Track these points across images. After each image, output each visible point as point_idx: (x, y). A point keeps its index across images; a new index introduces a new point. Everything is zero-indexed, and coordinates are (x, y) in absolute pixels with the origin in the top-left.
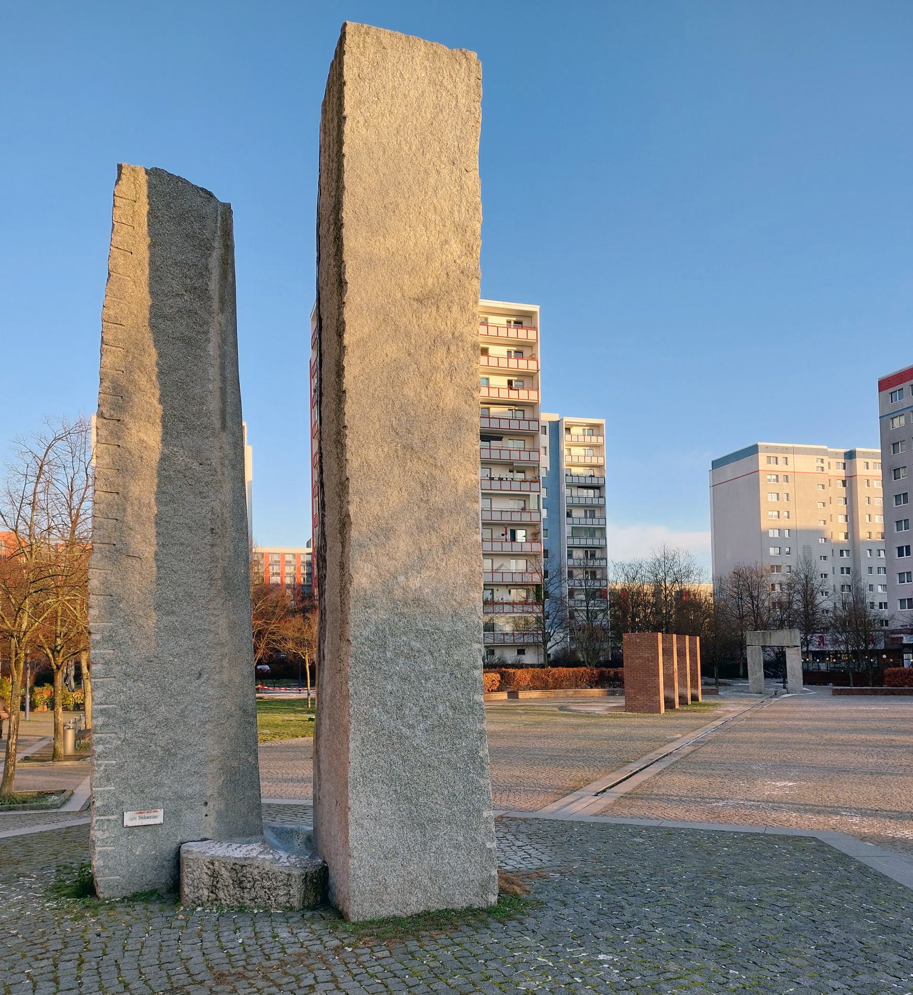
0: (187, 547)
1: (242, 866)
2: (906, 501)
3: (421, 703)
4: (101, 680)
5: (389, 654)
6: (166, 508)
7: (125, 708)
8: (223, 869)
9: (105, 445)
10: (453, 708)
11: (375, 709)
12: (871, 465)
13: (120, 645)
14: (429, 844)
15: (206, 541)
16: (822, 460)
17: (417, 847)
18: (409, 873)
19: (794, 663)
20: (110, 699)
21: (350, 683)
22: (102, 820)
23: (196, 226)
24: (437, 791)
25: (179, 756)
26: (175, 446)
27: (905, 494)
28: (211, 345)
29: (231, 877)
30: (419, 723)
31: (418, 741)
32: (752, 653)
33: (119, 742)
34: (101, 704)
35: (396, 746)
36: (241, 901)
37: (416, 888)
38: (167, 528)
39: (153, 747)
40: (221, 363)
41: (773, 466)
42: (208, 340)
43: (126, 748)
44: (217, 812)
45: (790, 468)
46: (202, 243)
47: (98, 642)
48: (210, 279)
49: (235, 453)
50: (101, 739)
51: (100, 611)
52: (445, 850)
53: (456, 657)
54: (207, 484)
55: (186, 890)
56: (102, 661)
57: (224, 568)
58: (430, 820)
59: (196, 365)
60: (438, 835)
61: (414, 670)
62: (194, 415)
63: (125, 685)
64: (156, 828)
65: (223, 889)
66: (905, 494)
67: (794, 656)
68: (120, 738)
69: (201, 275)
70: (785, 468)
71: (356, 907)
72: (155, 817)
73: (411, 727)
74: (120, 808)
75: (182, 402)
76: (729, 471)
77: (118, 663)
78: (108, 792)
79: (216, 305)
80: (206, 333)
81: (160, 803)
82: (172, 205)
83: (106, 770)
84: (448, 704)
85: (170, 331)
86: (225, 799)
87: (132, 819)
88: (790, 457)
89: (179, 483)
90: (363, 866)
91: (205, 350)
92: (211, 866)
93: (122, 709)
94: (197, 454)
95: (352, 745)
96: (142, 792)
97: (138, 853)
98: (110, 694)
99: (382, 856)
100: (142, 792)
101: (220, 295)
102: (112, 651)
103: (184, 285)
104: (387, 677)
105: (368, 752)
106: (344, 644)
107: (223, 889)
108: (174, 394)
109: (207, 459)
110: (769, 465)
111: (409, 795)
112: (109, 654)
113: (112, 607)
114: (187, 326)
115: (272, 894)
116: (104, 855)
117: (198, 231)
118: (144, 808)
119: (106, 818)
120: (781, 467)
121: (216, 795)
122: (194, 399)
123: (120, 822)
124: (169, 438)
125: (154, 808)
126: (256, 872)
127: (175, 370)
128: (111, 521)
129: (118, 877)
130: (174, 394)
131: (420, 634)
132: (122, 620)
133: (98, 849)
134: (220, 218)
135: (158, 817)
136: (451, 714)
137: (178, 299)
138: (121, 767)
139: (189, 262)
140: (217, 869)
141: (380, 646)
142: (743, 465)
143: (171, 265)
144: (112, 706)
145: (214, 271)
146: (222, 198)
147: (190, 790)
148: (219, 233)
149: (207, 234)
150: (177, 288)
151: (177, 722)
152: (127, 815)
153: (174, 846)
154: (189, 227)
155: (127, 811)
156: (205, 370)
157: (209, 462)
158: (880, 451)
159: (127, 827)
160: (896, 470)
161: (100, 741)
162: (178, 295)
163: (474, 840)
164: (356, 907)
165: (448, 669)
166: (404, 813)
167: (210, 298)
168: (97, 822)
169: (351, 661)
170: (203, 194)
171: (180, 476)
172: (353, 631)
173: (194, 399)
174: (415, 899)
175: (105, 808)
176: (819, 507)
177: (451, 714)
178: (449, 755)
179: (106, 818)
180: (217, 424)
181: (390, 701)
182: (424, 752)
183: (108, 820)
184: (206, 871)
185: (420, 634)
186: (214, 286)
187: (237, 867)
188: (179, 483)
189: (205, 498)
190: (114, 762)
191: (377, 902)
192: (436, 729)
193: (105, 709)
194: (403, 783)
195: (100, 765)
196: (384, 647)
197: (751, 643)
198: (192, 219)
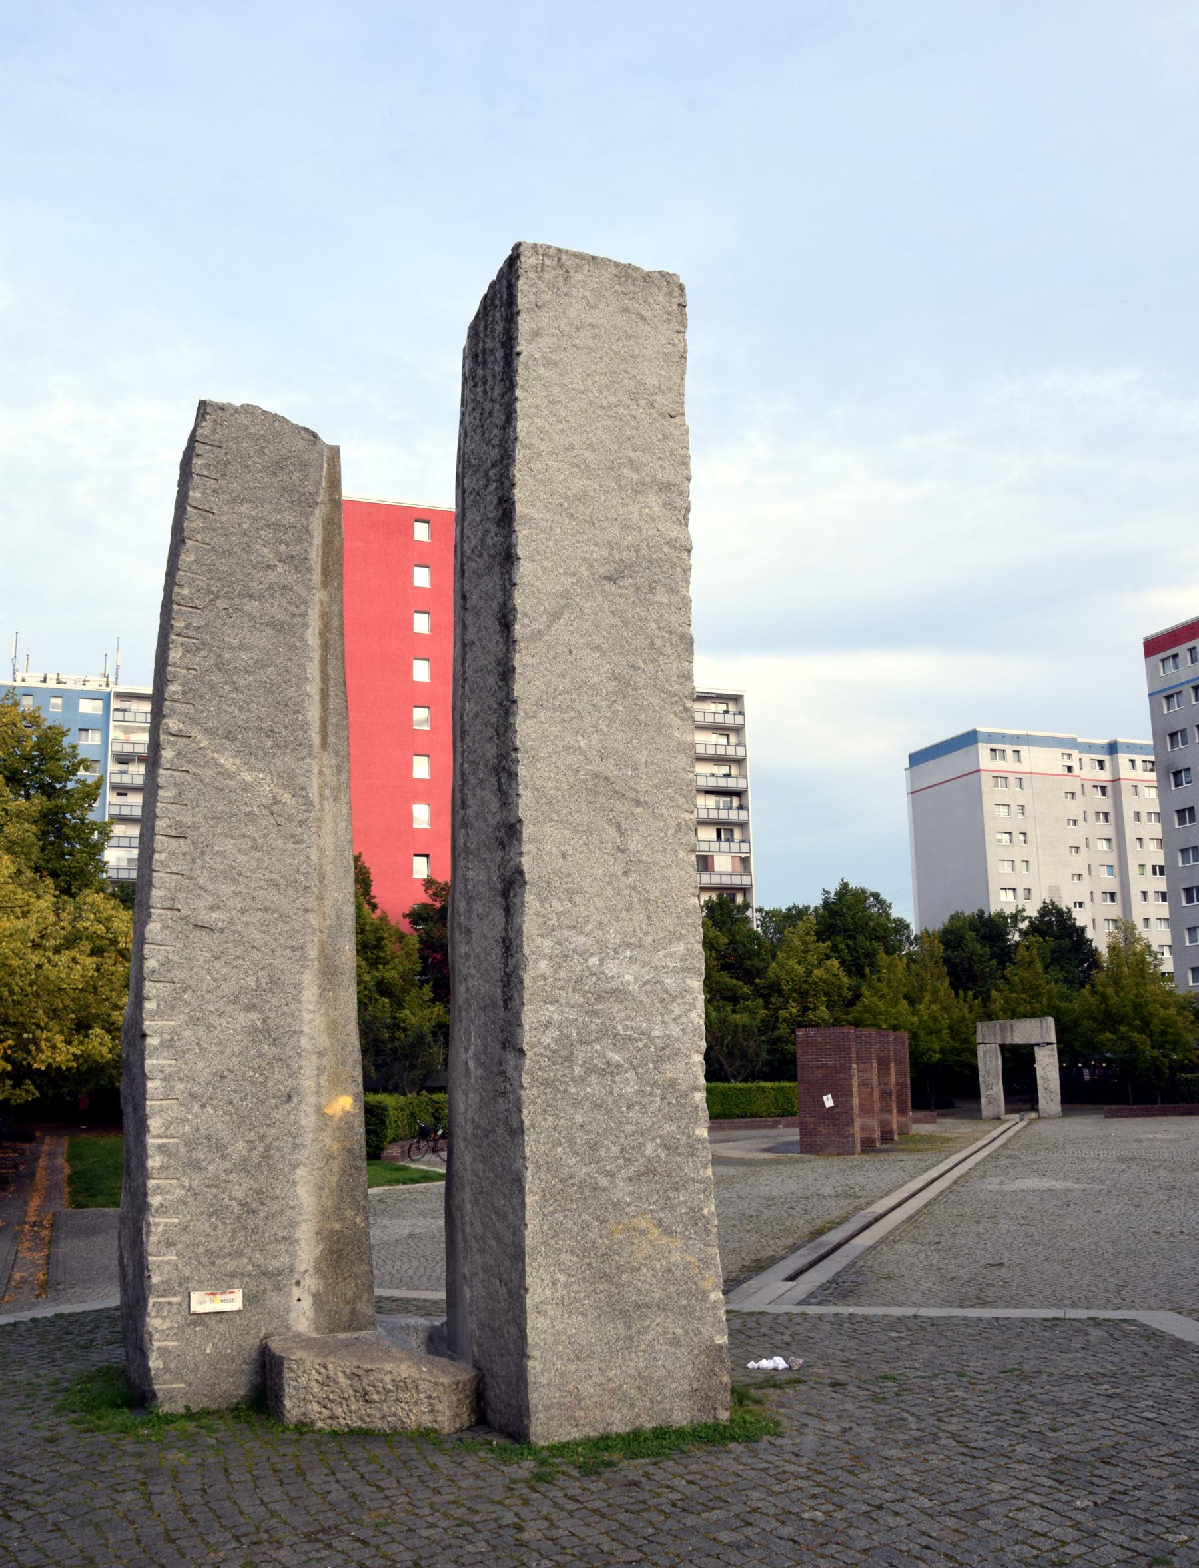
0: (274, 912)
1: (368, 1371)
2: (1192, 819)
3: (622, 1140)
4: (158, 1103)
5: (577, 1070)
6: (247, 858)
7: (190, 1144)
8: (340, 1374)
9: (170, 772)
10: (666, 1147)
11: (559, 1149)
12: (1139, 763)
13: (184, 1052)
14: (635, 1340)
15: (299, 905)
16: (1070, 755)
17: (620, 1345)
18: (610, 1380)
19: (1047, 1067)
20: (171, 1131)
21: (525, 1112)
22: (160, 1303)
23: (297, 476)
24: (646, 1265)
25: (262, 1214)
26: (260, 770)
27: (1191, 809)
28: (310, 631)
29: (351, 1386)
30: (620, 1168)
31: (620, 1195)
32: (985, 1056)
33: (183, 1192)
34: (159, 1136)
35: (589, 1202)
36: (368, 1420)
37: (619, 1401)
38: (247, 886)
39: (227, 1200)
40: (322, 655)
41: (998, 765)
42: (306, 626)
43: (190, 1200)
44: (314, 1296)
45: (1023, 767)
46: (303, 498)
47: (156, 1049)
48: (311, 544)
49: (339, 780)
50: (158, 1187)
51: (158, 1005)
52: (658, 1347)
53: (669, 1075)
54: (301, 823)
55: (288, 1403)
56: (161, 1076)
57: (322, 943)
58: (638, 1307)
59: (290, 659)
60: (649, 1326)
61: (612, 1093)
62: (286, 728)
63: (189, 1110)
64: (232, 1316)
65: (341, 1403)
66: (1191, 809)
67: (1047, 1060)
68: (184, 1187)
69: (300, 540)
70: (1017, 767)
71: (539, 1428)
72: (232, 1301)
73: (611, 1174)
74: (184, 1287)
75: (271, 710)
76: (936, 770)
77: (181, 1079)
78: (168, 1263)
79: (317, 577)
80: (304, 615)
81: (237, 1282)
82: (266, 451)
83: (165, 1232)
84: (658, 1141)
85: (258, 615)
86: (325, 1277)
87: (202, 1303)
88: (1024, 750)
89: (265, 823)
90: (548, 1371)
91: (302, 639)
92: (323, 1371)
93: (185, 1145)
94: (289, 781)
95: (529, 1199)
96: (213, 1264)
97: (208, 1351)
98: (171, 1123)
99: (572, 1356)
100: (213, 1264)
101: (323, 564)
102: (173, 1062)
103: (278, 553)
104: (576, 1104)
105: (551, 1209)
106: (510, 1056)
107: (341, 1403)
108: (262, 699)
109: (302, 789)
110: (994, 763)
111: (608, 1270)
112: (170, 1065)
113: (175, 999)
114: (280, 606)
115: (411, 1411)
116: (164, 1352)
117: (298, 483)
118: (220, 1285)
119: (167, 1300)
120: (1010, 764)
121: (311, 1271)
122: (287, 705)
123: (185, 1307)
124: (253, 760)
125: (229, 1288)
126: (387, 1378)
127: (264, 666)
128: (174, 877)
129: (182, 1386)
130: (262, 699)
131: (620, 1042)
132: (186, 1018)
133: (156, 1344)
134: (325, 466)
135: (234, 1301)
136: (663, 1155)
137: (270, 572)
138: (185, 1229)
139: (285, 523)
140: (331, 1373)
141: (566, 1059)
142: (954, 763)
143: (262, 529)
144: (172, 1140)
145: (316, 534)
146: (327, 438)
147: (276, 1264)
148: (324, 484)
149: (309, 487)
150: (268, 554)
151: (259, 1164)
152: (195, 1297)
153: (257, 1343)
154: (286, 478)
155: (194, 1290)
156: (302, 667)
157: (304, 793)
158: (1151, 743)
159: (195, 1314)
160: (1177, 774)
161: (159, 1190)
162: (269, 567)
163: (697, 1332)
164: (539, 1428)
165: (659, 1091)
166: (602, 1296)
167: (309, 570)
168: (154, 1305)
169: (526, 1079)
170: (306, 436)
171: (266, 812)
172: (528, 1037)
173: (287, 705)
174: (619, 1416)
175: (165, 1286)
176: (1100, 848)
177: (663, 1155)
178: (661, 1215)
179: (167, 1300)
180: (316, 740)
181: (580, 1137)
182: (628, 1209)
183: (169, 1303)
184: (316, 1376)
185: (620, 1042)
186: (315, 555)
187: (360, 1372)
188: (265, 823)
189: (298, 843)
190: (175, 1221)
191: (567, 1420)
192: (643, 1178)
193: (164, 1145)
194: (599, 1254)
195: (158, 1225)
196: (569, 1059)
197: (984, 1037)
198: (291, 468)
